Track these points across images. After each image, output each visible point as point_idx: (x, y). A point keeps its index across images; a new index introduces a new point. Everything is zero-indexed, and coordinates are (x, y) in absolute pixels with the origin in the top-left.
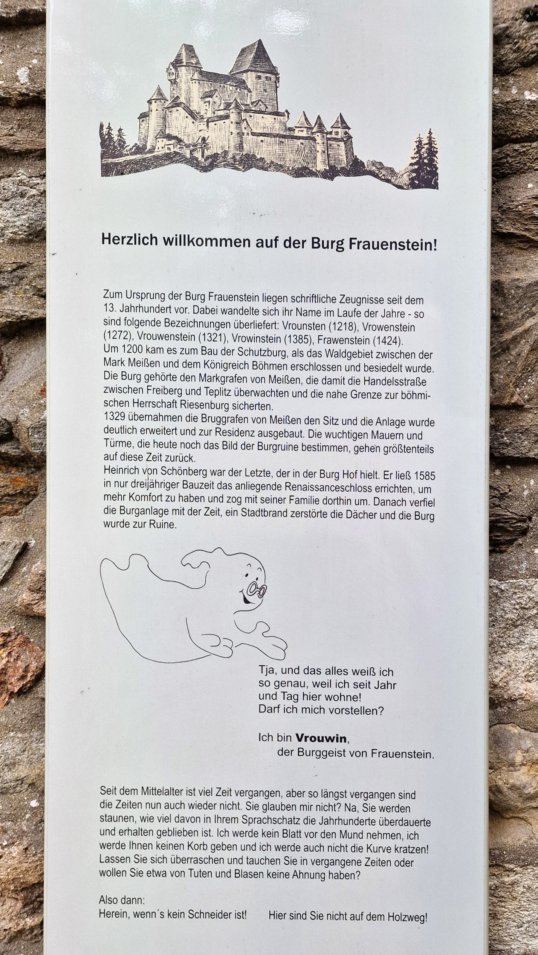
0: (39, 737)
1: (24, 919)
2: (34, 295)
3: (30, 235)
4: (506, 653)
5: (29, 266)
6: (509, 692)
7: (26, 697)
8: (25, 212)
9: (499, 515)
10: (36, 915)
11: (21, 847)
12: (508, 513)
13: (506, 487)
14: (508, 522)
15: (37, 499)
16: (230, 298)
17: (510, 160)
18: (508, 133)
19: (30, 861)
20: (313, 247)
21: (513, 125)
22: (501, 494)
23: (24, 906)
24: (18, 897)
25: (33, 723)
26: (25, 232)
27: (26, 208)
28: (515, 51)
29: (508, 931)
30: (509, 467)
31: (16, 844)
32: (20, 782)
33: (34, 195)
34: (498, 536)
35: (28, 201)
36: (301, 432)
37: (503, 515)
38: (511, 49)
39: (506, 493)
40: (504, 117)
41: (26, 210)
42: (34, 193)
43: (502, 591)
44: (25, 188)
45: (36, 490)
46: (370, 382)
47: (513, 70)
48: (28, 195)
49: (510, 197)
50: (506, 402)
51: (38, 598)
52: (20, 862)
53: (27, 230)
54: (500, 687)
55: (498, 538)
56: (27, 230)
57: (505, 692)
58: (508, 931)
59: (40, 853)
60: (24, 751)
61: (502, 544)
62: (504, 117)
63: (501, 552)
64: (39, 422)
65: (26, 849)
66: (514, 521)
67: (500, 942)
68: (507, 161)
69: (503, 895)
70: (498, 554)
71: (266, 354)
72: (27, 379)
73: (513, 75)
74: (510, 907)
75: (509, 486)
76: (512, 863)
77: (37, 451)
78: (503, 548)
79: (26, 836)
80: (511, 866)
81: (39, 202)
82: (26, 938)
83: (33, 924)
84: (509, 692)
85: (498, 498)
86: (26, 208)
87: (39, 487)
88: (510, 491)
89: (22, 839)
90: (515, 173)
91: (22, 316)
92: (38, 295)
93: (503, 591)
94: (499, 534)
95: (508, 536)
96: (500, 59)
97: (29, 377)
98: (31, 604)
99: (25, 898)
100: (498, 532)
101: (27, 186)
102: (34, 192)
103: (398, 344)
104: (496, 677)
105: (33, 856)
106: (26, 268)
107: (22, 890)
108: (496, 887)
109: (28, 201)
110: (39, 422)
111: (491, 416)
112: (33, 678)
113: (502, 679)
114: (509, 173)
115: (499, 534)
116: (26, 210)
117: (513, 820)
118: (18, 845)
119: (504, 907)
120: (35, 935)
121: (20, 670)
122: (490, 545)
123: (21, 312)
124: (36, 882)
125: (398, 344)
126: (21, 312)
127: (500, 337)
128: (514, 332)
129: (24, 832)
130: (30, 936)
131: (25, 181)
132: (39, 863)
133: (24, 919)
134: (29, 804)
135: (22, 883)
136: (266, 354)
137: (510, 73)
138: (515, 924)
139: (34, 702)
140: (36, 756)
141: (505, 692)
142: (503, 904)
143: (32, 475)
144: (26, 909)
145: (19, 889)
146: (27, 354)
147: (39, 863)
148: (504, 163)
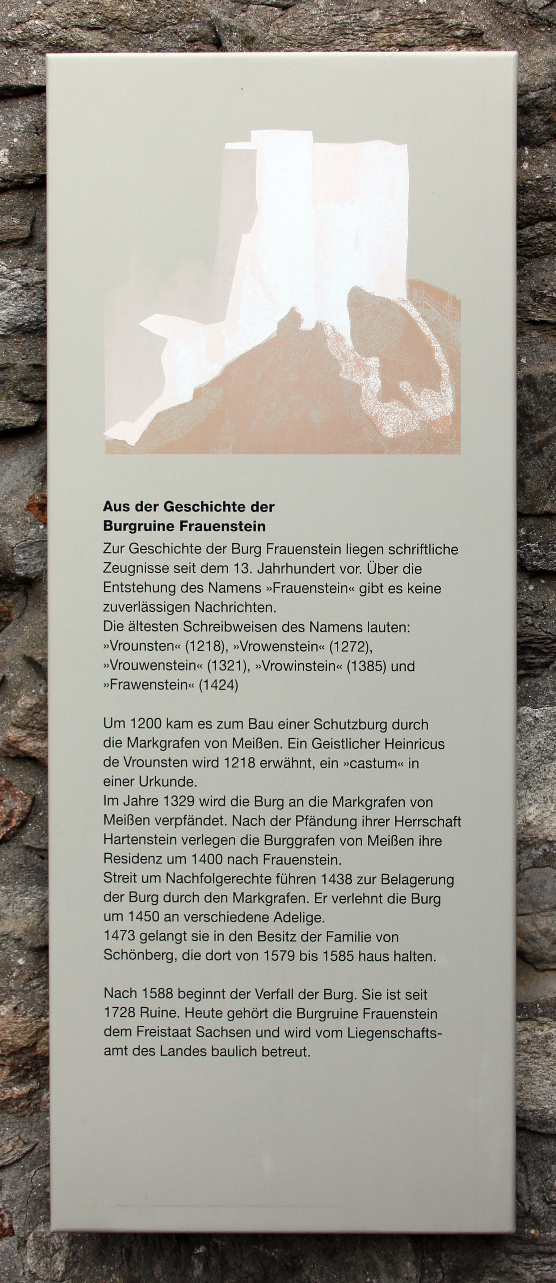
0: (23, 890)
1: (11, 1088)
2: (19, 401)
3: (9, 330)
4: (541, 789)
5: (10, 367)
6: (544, 832)
7: (9, 847)
8: (5, 306)
9: (532, 635)
10: (23, 1084)
11: (11, 1007)
12: (542, 633)
13: (541, 603)
14: (543, 643)
15: (11, 626)
16: (298, 550)
17: (542, 240)
18: (539, 212)
19: (19, 1021)
20: (105, 529)
21: (544, 203)
22: (534, 612)
23: (11, 1074)
24: (5, 1063)
25: (16, 875)
26: (4, 328)
27: (7, 302)
28: (546, 123)
29: (541, 1089)
30: (543, 582)
31: (4, 1002)
32: (6, 938)
33: (15, 288)
34: (532, 659)
35: (8, 295)
36: (305, 1050)
37: (537, 635)
38: (542, 120)
39: (540, 611)
40: (534, 195)
41: (6, 304)
42: (15, 286)
43: (536, 719)
44: (5, 280)
45: (9, 616)
46: (114, 840)
47: (544, 143)
48: (8, 289)
49: (543, 280)
50: (539, 509)
51: (24, 734)
52: (9, 1023)
53: (6, 325)
54: (535, 826)
55: (532, 661)
56: (6, 325)
57: (540, 831)
58: (541, 1089)
59: (30, 1013)
60: (9, 905)
61: (537, 667)
62: (534, 195)
63: (536, 676)
64: (26, 541)
65: (15, 1008)
66: (549, 641)
67: (533, 1101)
68: (540, 242)
69: (536, 1050)
70: (533, 679)
71: (357, 726)
72: (8, 492)
73: (545, 148)
74: (543, 1063)
75: (543, 602)
76: (547, 1016)
77: (21, 573)
78: (538, 672)
79: (15, 995)
80: (545, 1019)
81: (21, 295)
82: (12, 1110)
83: (20, 1093)
84: (544, 832)
85: (531, 616)
86: (7, 302)
87: (13, 612)
88: (544, 608)
89: (10, 998)
90: (548, 254)
91: (7, 425)
92: (23, 401)
93: (537, 719)
94: (533, 656)
95: (543, 658)
96: (530, 131)
97: (10, 489)
98: (18, 742)
99: (12, 1065)
100: (532, 654)
101: (7, 278)
102: (14, 285)
103: (235, 689)
104: (530, 814)
105: (23, 1016)
106: (7, 370)
107: (9, 1056)
108: (529, 1041)
109: (8, 295)
110: (26, 541)
111: (519, 526)
112: (18, 824)
113: (536, 816)
114: (541, 254)
115: (533, 656)
116: (6, 304)
117: (548, 972)
118: (7, 1004)
119: (538, 1064)
120: (22, 1107)
121: (4, 816)
122: (519, 668)
123: (5, 421)
124: (25, 1045)
125: (235, 689)
126: (5, 421)
127: (532, 438)
128: (545, 433)
129: (12, 990)
130: (16, 1108)
131: (5, 273)
132: (29, 1024)
133: (11, 1088)
134: (16, 962)
135: (11, 1046)
136: (357, 726)
137: (542, 144)
138: (549, 1082)
139: (17, 851)
140: (21, 911)
141: (540, 831)
142: (536, 1061)
143: (6, 599)
144: (13, 1077)
145: (6, 1054)
146: (7, 465)
147: (29, 1024)
148: (536, 244)
